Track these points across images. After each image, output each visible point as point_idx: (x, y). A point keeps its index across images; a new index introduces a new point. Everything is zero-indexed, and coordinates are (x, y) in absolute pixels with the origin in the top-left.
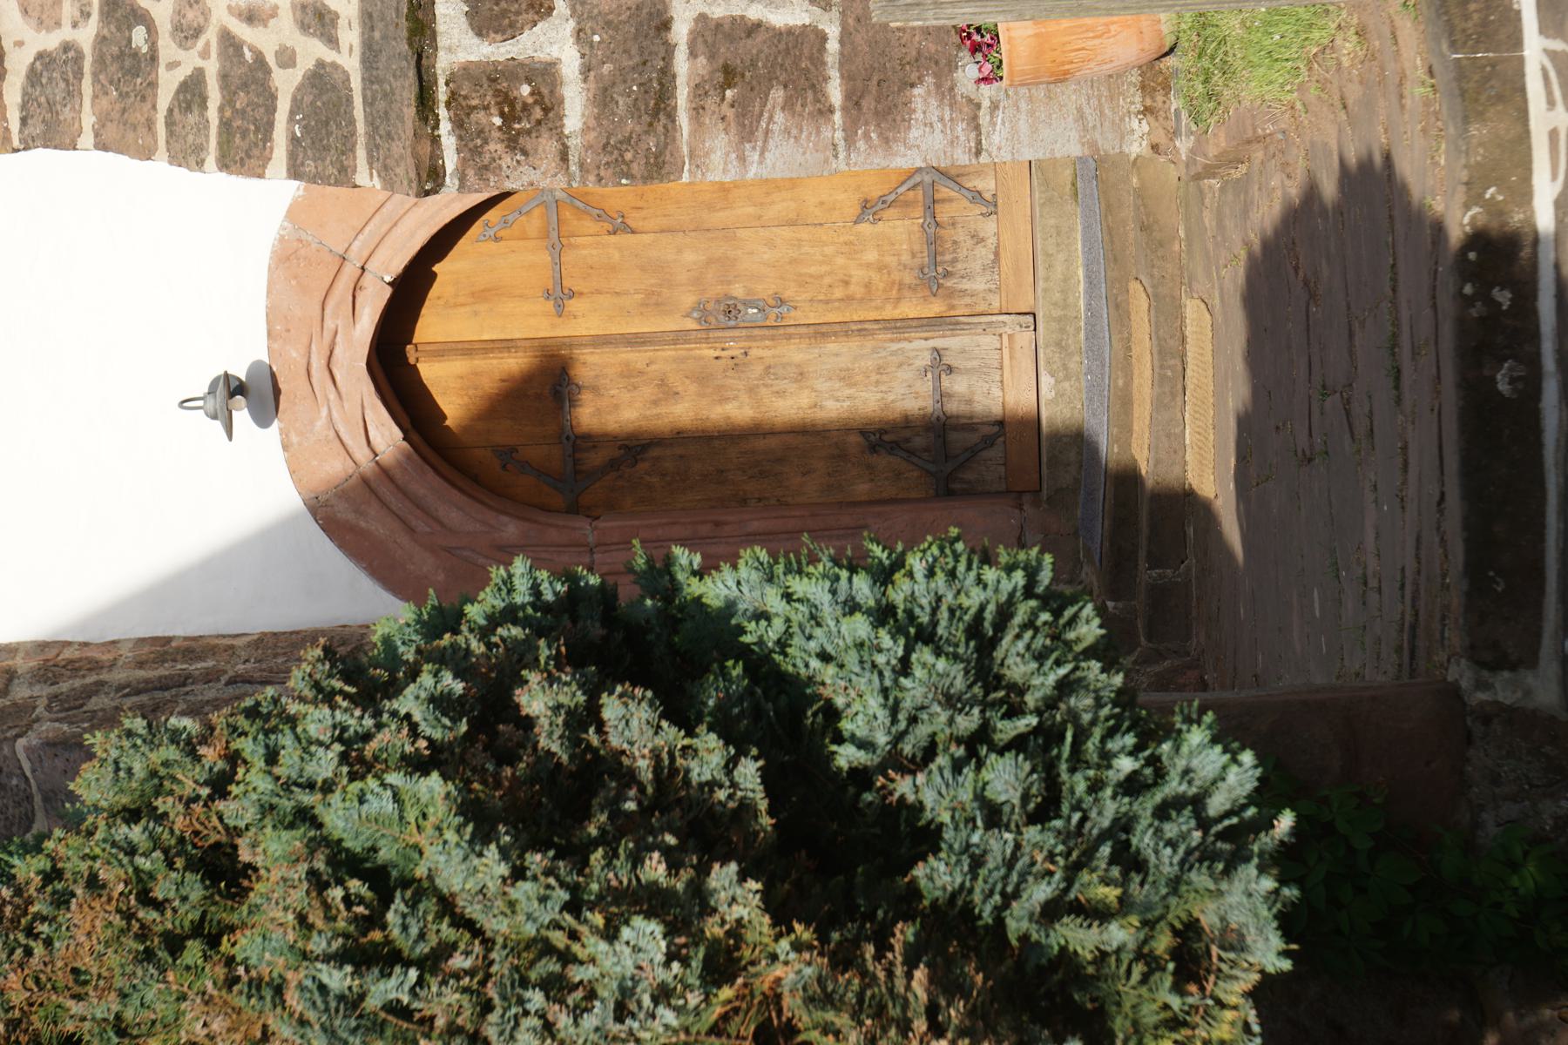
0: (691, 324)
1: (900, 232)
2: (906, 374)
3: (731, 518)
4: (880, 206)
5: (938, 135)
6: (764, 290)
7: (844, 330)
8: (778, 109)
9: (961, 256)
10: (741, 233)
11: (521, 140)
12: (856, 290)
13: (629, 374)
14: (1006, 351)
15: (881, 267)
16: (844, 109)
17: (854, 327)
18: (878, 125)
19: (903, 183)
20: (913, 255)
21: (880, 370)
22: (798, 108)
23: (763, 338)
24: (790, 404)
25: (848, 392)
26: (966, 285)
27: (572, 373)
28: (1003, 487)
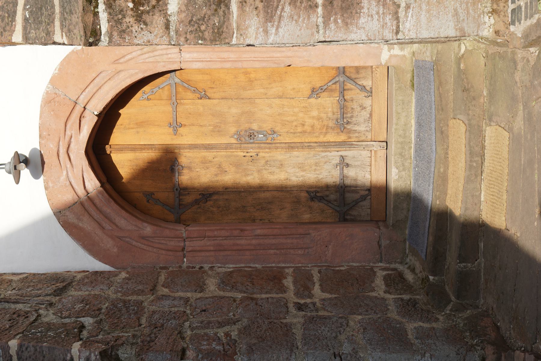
0: (233, 141)
1: (329, 102)
2: (327, 167)
3: (248, 228)
4: (320, 91)
5: (375, 22)
6: (267, 127)
7: (302, 146)
8: (287, 4)
9: (355, 115)
10: (257, 101)
11: (144, 17)
12: (308, 128)
13: (205, 162)
14: (373, 158)
15: (319, 119)
16: (324, 5)
17: (306, 145)
18: (342, 15)
19: (330, 81)
20: (334, 114)
21: (316, 164)
22: (298, 4)
23: (265, 148)
24: (276, 176)
25: (302, 173)
26: (356, 128)
27: (180, 160)
28: (369, 218)
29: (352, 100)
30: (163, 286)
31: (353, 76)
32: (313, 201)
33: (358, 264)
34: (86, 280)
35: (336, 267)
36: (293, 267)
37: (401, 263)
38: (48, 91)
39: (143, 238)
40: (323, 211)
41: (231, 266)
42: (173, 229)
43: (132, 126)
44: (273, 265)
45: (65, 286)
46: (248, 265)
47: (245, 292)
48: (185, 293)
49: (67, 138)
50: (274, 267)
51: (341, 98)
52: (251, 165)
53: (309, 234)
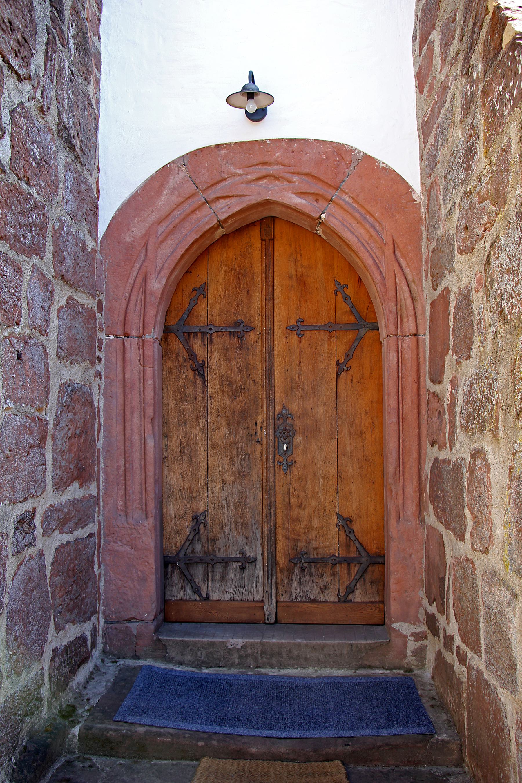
0: (278, 408)
1: (331, 542)
3: (156, 428)
6: (298, 455)
10: (334, 443)
15: (309, 528)
17: (272, 511)
19: (361, 544)
20: (315, 549)
21: (245, 524)
26: (295, 581)
29: (334, 574)
30: (70, 298)
31: (368, 577)
32: (193, 520)
33: (102, 588)
34: (83, 187)
35: (98, 557)
36: (99, 495)
37: (104, 652)
38: (354, 151)
39: (145, 280)
40: (178, 533)
41: (102, 404)
42: (156, 321)
43: (300, 269)
44: (102, 465)
45: (74, 150)
46: (102, 428)
47: (56, 425)
48: (56, 330)
49: (289, 176)
50: (99, 467)
51: (337, 559)
52: (243, 434)
53: (147, 517)
